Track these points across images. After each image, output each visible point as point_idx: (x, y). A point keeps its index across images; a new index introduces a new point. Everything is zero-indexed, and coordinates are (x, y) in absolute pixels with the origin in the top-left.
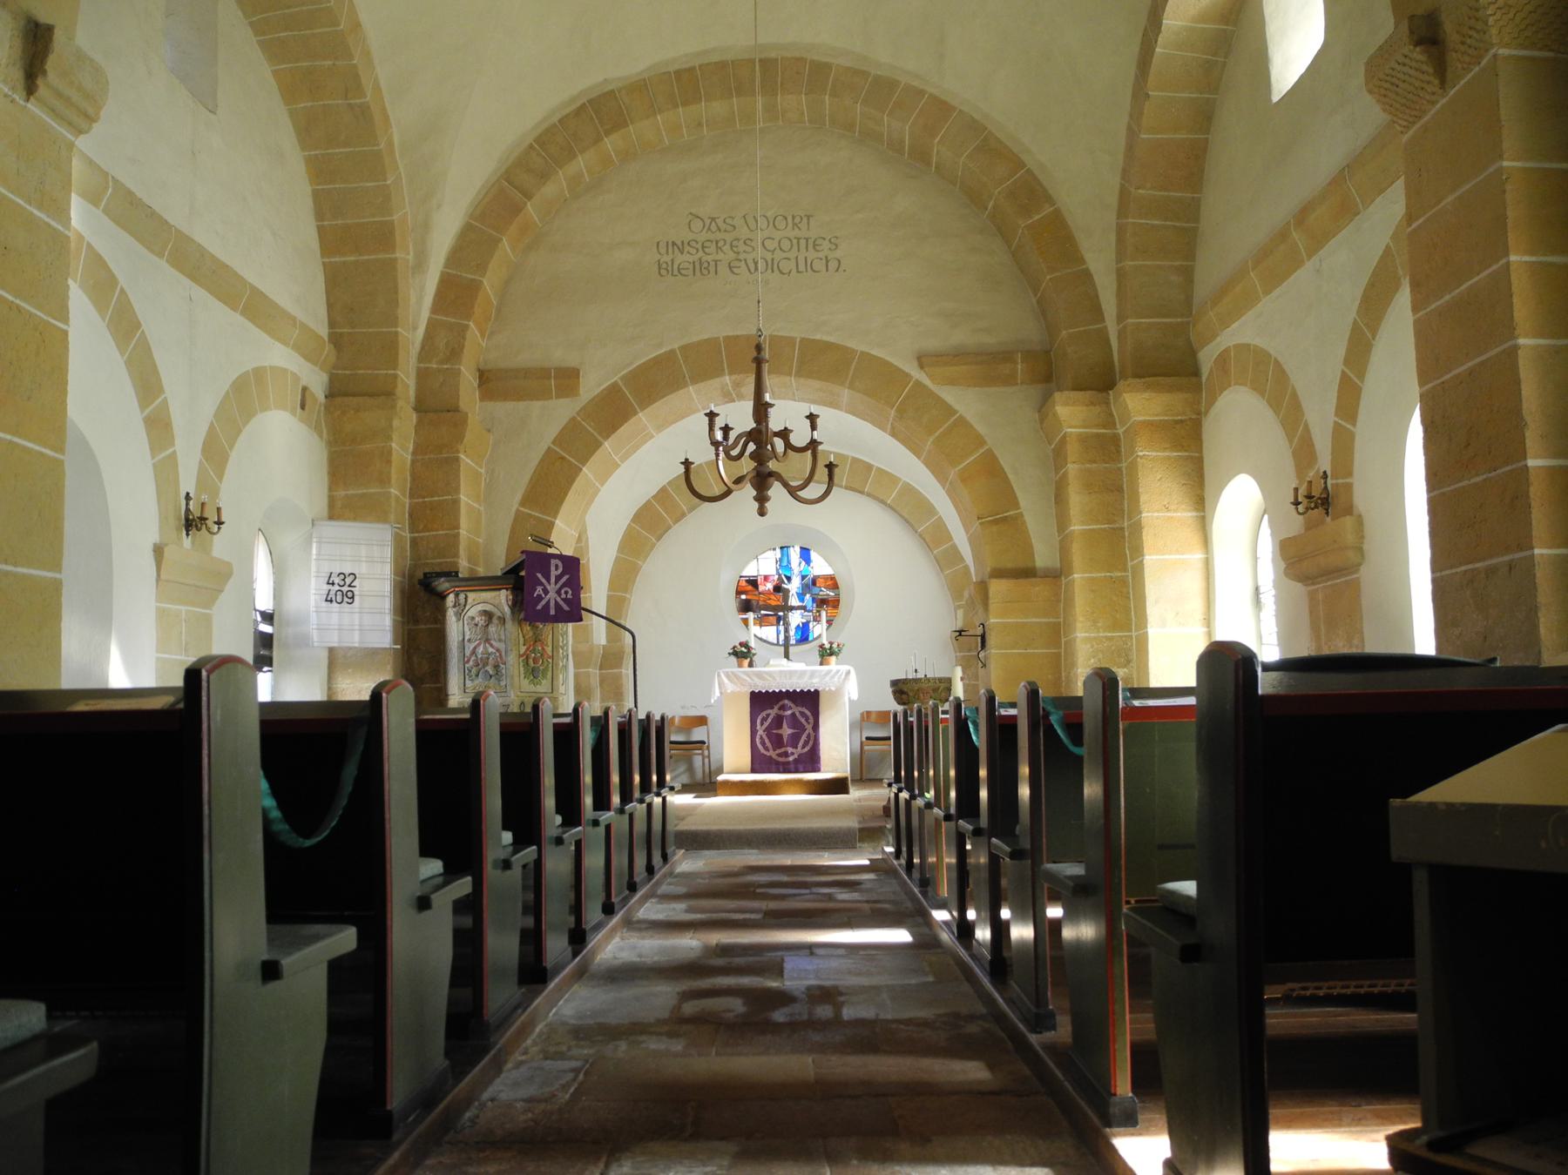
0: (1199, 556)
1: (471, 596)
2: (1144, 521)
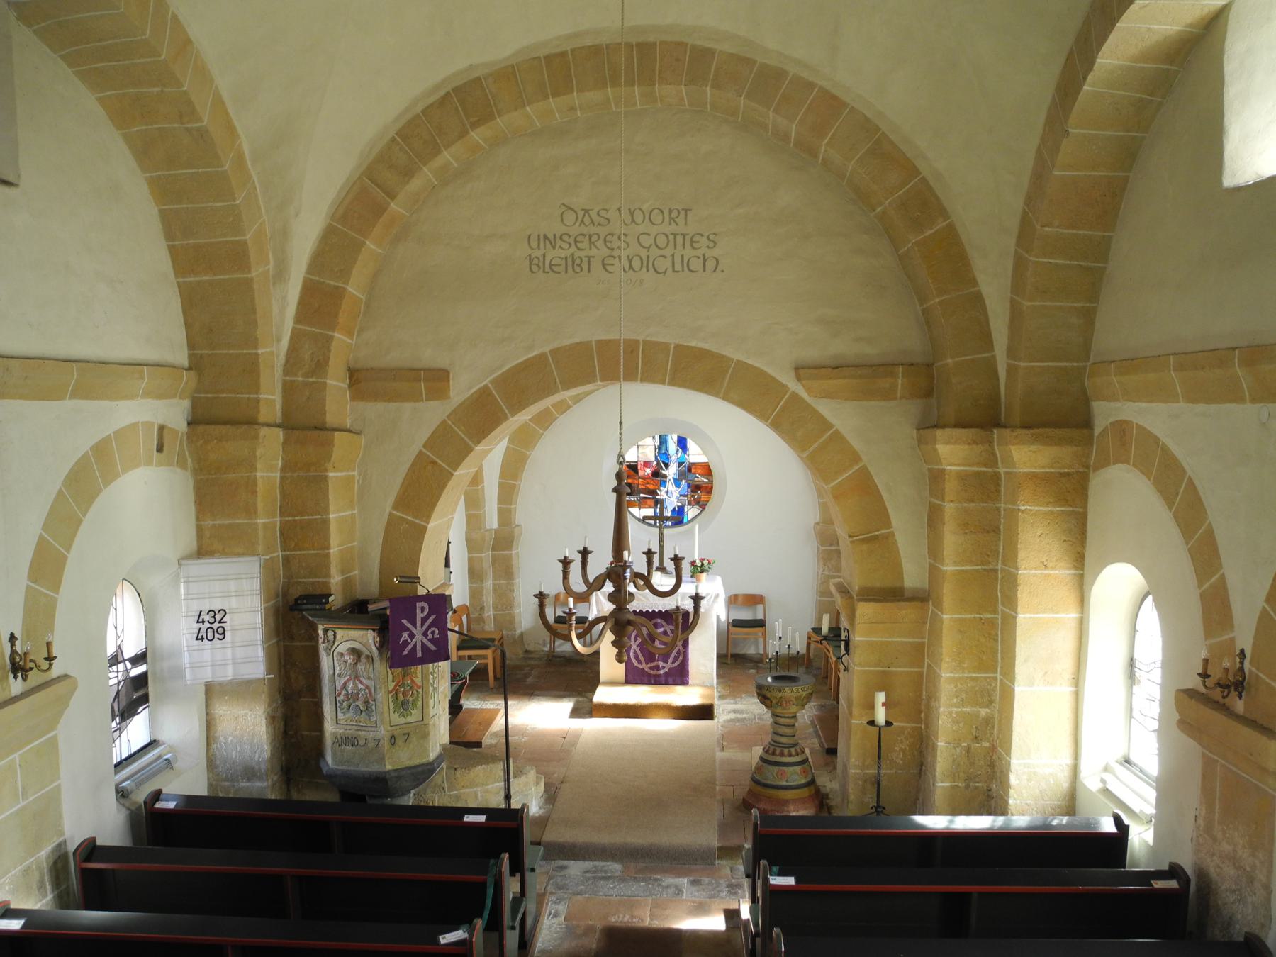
0: (1074, 615)
1: (340, 633)
2: (1020, 579)
